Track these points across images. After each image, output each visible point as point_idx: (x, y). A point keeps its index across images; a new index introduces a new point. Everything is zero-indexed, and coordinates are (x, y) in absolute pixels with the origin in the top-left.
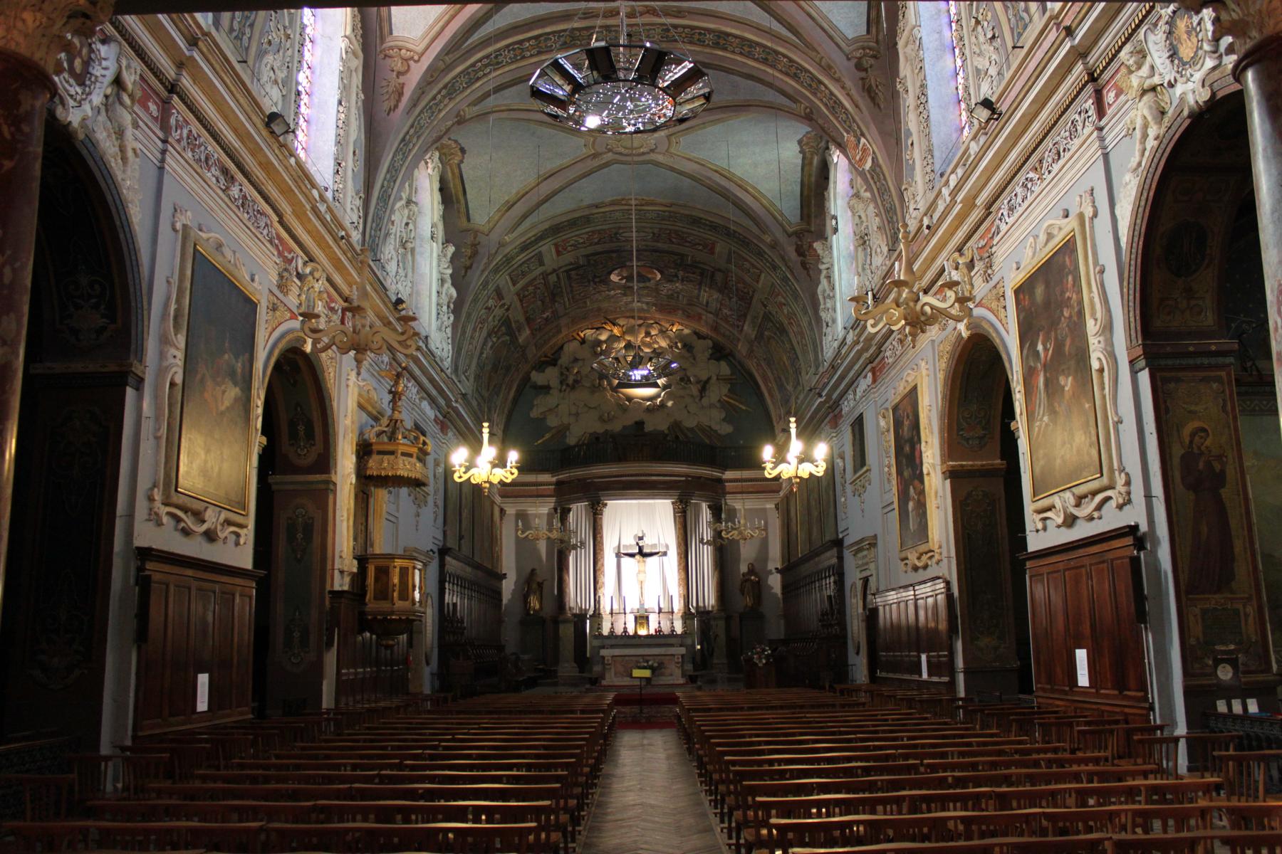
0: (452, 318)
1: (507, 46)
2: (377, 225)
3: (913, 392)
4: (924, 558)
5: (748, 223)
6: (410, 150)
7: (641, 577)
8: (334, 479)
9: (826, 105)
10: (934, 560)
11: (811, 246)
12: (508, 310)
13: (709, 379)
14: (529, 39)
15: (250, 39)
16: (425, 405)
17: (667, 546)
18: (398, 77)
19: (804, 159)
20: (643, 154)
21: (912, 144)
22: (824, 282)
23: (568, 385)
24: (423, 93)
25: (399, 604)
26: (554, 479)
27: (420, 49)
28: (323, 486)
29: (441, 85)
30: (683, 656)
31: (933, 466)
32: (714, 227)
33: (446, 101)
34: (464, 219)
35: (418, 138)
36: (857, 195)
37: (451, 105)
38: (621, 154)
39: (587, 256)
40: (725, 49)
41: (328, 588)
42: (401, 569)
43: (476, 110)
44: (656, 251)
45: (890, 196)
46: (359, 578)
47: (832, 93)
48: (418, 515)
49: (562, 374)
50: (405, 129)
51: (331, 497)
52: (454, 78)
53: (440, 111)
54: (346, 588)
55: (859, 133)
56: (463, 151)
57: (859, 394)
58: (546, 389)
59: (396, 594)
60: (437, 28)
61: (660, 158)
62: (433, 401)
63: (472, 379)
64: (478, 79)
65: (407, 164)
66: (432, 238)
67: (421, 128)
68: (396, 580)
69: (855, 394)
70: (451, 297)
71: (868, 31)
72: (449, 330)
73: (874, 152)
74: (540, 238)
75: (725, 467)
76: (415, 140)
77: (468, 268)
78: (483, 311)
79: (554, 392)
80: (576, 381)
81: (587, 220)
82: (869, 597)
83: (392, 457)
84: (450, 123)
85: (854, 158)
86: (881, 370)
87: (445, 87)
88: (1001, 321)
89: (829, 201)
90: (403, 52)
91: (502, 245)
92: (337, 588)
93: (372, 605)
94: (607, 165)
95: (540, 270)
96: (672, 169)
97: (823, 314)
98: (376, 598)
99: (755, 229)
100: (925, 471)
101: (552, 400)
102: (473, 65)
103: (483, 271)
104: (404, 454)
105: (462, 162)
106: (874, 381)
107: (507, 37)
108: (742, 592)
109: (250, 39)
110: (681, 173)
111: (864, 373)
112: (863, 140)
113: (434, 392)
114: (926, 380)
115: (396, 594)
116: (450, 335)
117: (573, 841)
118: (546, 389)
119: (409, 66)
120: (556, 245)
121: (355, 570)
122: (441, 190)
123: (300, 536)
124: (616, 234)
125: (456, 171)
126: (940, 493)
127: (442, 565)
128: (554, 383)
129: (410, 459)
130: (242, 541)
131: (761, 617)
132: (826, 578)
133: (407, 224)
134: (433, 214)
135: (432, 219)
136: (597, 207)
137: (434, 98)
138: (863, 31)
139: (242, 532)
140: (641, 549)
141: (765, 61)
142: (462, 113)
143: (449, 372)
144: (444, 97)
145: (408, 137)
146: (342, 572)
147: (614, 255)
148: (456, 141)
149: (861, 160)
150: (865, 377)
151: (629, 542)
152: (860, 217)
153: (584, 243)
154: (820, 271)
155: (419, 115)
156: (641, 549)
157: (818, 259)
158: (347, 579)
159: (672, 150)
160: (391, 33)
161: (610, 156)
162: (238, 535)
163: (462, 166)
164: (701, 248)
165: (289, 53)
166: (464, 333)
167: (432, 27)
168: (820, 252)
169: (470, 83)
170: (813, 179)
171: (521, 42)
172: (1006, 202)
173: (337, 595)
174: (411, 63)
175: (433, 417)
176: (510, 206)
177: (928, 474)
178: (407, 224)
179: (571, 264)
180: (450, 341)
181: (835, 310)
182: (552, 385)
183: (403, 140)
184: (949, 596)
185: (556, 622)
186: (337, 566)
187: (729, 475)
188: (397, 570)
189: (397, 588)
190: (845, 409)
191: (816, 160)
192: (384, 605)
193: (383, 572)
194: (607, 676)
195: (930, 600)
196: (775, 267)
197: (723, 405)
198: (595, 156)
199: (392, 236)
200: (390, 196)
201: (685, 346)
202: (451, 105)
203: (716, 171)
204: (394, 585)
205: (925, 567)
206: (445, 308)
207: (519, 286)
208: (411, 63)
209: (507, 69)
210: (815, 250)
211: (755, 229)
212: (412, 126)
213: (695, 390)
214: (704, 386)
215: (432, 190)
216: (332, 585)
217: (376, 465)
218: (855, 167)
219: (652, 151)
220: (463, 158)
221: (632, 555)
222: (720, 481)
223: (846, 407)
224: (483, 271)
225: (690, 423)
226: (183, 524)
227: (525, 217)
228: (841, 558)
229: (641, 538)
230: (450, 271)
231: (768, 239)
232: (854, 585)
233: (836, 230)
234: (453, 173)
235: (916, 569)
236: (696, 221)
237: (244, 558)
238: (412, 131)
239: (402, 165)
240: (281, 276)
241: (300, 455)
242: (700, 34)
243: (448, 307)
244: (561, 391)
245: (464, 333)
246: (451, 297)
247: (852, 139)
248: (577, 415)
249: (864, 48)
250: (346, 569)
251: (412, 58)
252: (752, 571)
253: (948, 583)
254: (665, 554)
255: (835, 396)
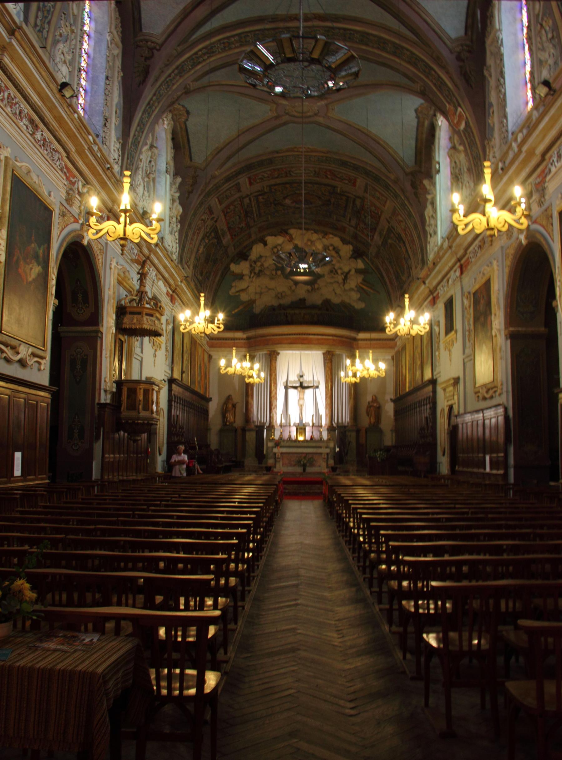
0: (179, 226)
1: (220, 40)
2: (131, 161)
3: (487, 285)
4: (491, 392)
5: (378, 164)
6: (153, 111)
7: (301, 402)
8: (101, 330)
9: (435, 85)
10: (497, 393)
11: (421, 182)
12: (216, 221)
13: (350, 271)
14: (233, 36)
15: (48, 32)
16: (161, 283)
17: (319, 382)
18: (145, 60)
19: (418, 122)
20: (310, 116)
21: (493, 113)
22: (429, 207)
23: (255, 273)
24: (162, 72)
25: (143, 414)
26: (245, 336)
27: (160, 41)
28: (94, 334)
29: (174, 67)
30: (328, 454)
31: (499, 331)
32: (356, 168)
33: (178, 77)
34: (188, 160)
35: (159, 103)
36: (454, 148)
37: (181, 81)
38: (294, 116)
39: (270, 186)
40: (367, 45)
41: (97, 401)
42: (144, 390)
43: (198, 84)
44: (316, 183)
45: (477, 148)
46: (117, 395)
47: (439, 77)
48: (155, 356)
49: (251, 266)
50: (150, 97)
51: (99, 341)
52: (184, 62)
53: (173, 84)
54: (108, 401)
55: (456, 104)
56: (188, 113)
57: (450, 282)
58: (240, 277)
59: (141, 407)
60: (172, 27)
61: (321, 120)
62: (166, 281)
63: (191, 267)
64: (200, 63)
65: (151, 120)
66: (167, 171)
67: (161, 96)
68: (141, 398)
69: (448, 281)
70: (179, 212)
71: (466, 33)
72: (177, 234)
73: (467, 118)
74: (238, 173)
75: (359, 329)
76: (156, 104)
77: (190, 192)
78: (200, 222)
79: (246, 278)
80: (260, 271)
81: (271, 161)
82: (453, 418)
83: (139, 316)
84: (179, 93)
85: (453, 121)
86: (466, 266)
87: (177, 68)
88: (549, 234)
89: (435, 151)
90: (149, 43)
91: (213, 177)
92: (102, 401)
93: (125, 413)
94: (285, 124)
95: (238, 195)
96: (329, 128)
97: (427, 228)
98: (128, 409)
99: (383, 170)
100: (494, 334)
101: (243, 285)
102: (196, 53)
103: (200, 195)
104: (147, 314)
105: (187, 120)
106: (462, 273)
107: (219, 34)
108: (368, 414)
109: (48, 32)
110: (334, 130)
111: (454, 269)
112: (459, 109)
113: (166, 275)
114: (496, 273)
115: (141, 407)
116: (177, 237)
117: (249, 585)
118: (240, 277)
119: (153, 53)
120: (250, 179)
121: (114, 390)
122: (173, 139)
123: (79, 367)
124: (290, 171)
125: (183, 127)
126: (503, 348)
127: (170, 390)
128: (246, 272)
129: (151, 318)
130: (42, 368)
131: (381, 432)
132: (424, 405)
133: (150, 162)
134: (167, 155)
135: (167, 159)
136: (277, 152)
137: (169, 76)
138: (462, 32)
139: (43, 362)
140: (301, 384)
141: (394, 54)
142: (188, 86)
143: (176, 262)
144: (176, 75)
145: (152, 102)
146: (106, 391)
147: (288, 186)
148: (183, 106)
149: (457, 123)
150: (455, 271)
151: (293, 378)
152: (455, 163)
153: (268, 177)
154: (427, 200)
155: (159, 87)
156: (301, 384)
157: (426, 192)
158: (109, 396)
159: (329, 115)
160: (141, 30)
161: (286, 118)
162: (39, 363)
163: (188, 123)
164: (347, 182)
165: (74, 42)
166: (187, 236)
167: (169, 26)
168: (428, 187)
169: (194, 65)
170: (424, 136)
171: (228, 38)
172: (556, 152)
173: (103, 406)
174: (155, 51)
175: (165, 292)
176: (219, 151)
177: (496, 336)
178: (150, 162)
179: (259, 191)
180: (177, 241)
181: (436, 226)
182: (244, 273)
183: (149, 104)
184: (506, 417)
185: (244, 430)
186: (102, 387)
187: (361, 335)
188: (142, 391)
189: (142, 403)
190: (441, 293)
191: (426, 123)
192: (133, 414)
193: (132, 392)
194: (278, 465)
195: (493, 420)
196: (396, 196)
197: (359, 289)
198: (277, 118)
199: (141, 169)
200: (139, 142)
201: (334, 249)
202: (181, 81)
203: (359, 130)
204: (140, 401)
205: (492, 397)
206: (174, 219)
207: (224, 205)
208: (155, 51)
209: (219, 56)
210: (424, 185)
211: (383, 170)
212: (154, 95)
213: (340, 278)
214: (346, 276)
215: (167, 138)
216: (99, 399)
217: (127, 321)
218: (454, 128)
219: (316, 114)
220: (188, 117)
221: (295, 388)
222: (355, 339)
223: (441, 291)
224: (200, 195)
225: (336, 300)
226: (4, 355)
227: (229, 158)
228: (434, 392)
229: (302, 376)
230: (178, 195)
231: (392, 177)
232: (443, 410)
233: (438, 172)
234: (181, 128)
235: (485, 399)
236: (344, 164)
237: (44, 379)
238: (154, 98)
239: (147, 121)
240: (68, 193)
241: (79, 313)
242: (350, 34)
243: (177, 219)
244: (250, 277)
245: (187, 236)
246: (179, 212)
247: (452, 108)
248: (261, 294)
249: (462, 45)
250: (108, 389)
251: (155, 48)
252: (375, 399)
253: (506, 409)
254: (317, 387)
255: (434, 283)
